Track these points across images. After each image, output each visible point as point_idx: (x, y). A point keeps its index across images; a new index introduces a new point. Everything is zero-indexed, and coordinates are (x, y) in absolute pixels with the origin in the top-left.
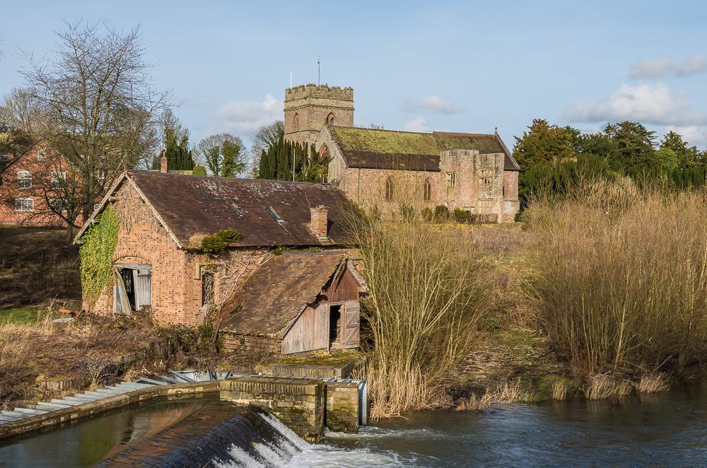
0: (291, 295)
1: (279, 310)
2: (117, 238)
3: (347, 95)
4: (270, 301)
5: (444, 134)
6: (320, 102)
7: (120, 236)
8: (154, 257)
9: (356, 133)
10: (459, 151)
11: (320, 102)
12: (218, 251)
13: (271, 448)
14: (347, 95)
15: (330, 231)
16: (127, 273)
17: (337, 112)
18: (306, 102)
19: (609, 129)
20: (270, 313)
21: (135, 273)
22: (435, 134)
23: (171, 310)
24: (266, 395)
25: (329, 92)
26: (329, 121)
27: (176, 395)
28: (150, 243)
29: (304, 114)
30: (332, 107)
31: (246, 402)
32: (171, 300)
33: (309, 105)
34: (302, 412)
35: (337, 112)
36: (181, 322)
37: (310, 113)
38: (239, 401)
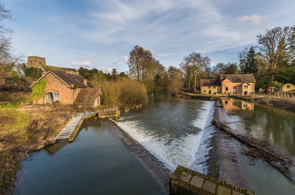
0: (92, 96)
1: (91, 99)
2: (46, 86)
3: (44, 59)
4: (87, 97)
5: (65, 68)
6: (38, 60)
7: (47, 85)
8: (59, 90)
9: (48, 66)
10: (70, 71)
11: (38, 60)
12: (74, 88)
13: (200, 121)
14: (44, 59)
15: (225, 77)
16: (51, 94)
17: (42, 62)
18: (34, 60)
19: (92, 69)
20: (89, 100)
21: (53, 94)
22: (63, 68)
23: (66, 101)
24: (108, 115)
25: (41, 58)
26: (40, 64)
27: (87, 118)
28: (58, 87)
29: (34, 62)
30: (41, 61)
31: (104, 117)
32: (66, 99)
33: (35, 60)
34: (115, 117)
35: (42, 62)
36: (69, 103)
37: (35, 62)
38: (103, 117)
